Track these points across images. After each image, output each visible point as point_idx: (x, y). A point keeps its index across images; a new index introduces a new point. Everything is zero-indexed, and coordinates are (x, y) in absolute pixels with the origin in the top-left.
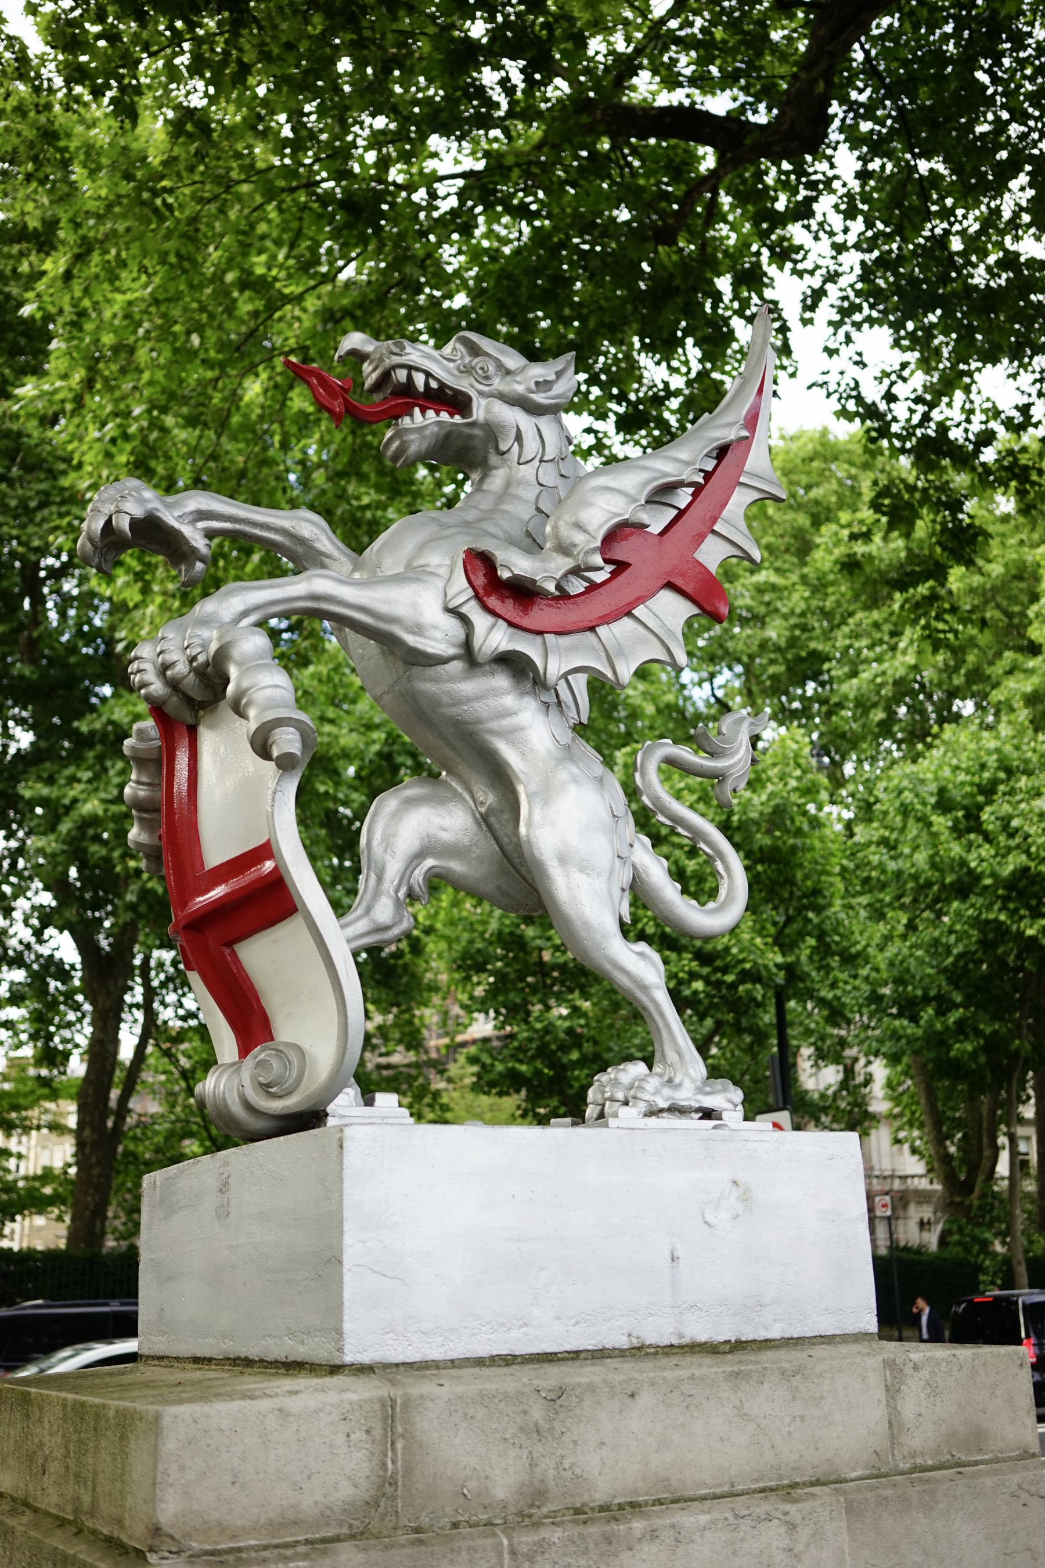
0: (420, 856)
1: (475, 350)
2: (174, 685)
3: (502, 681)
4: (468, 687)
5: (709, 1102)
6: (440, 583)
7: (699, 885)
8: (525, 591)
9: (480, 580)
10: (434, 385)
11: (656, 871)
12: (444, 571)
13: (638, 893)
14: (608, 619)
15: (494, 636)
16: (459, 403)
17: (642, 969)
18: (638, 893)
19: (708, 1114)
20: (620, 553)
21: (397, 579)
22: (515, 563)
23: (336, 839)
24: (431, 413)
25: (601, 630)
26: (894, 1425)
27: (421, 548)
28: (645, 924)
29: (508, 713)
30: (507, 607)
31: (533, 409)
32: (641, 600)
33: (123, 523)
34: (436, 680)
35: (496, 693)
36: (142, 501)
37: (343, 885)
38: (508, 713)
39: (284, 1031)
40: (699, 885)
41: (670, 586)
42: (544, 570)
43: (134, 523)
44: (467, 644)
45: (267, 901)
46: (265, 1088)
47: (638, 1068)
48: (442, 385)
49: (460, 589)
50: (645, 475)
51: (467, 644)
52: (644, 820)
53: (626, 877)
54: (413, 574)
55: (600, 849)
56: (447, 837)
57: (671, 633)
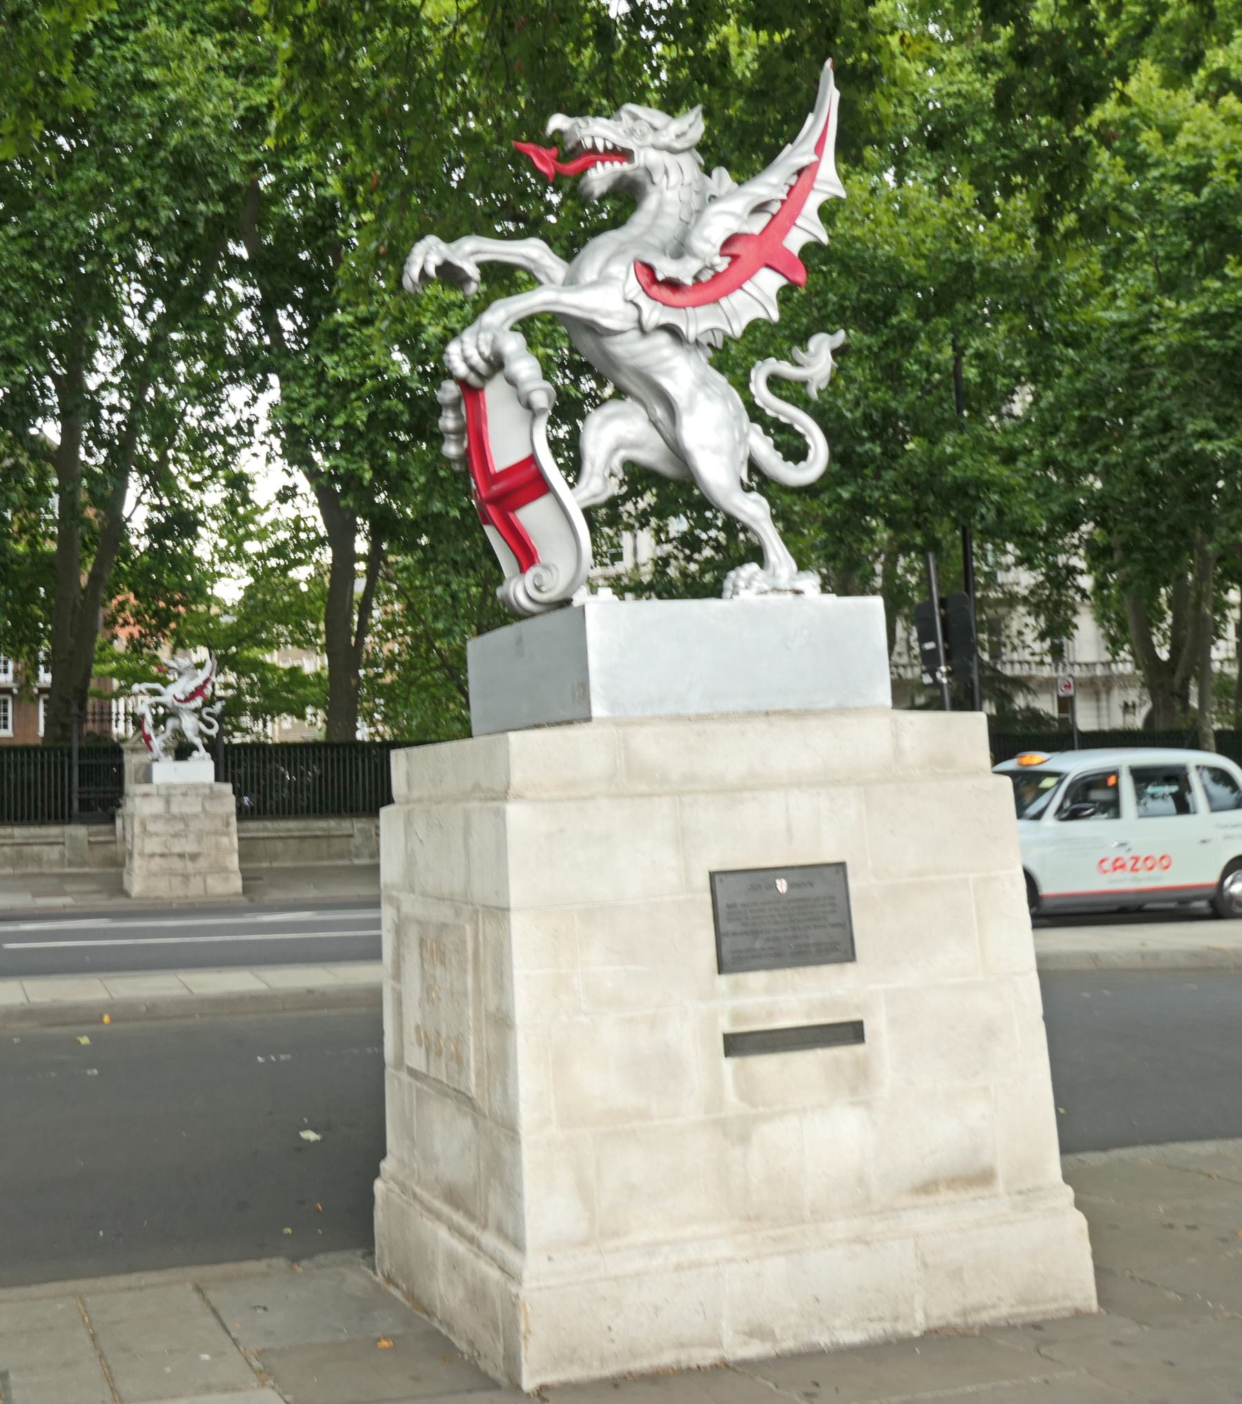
0: (616, 450)
1: (635, 118)
2: (472, 368)
3: (664, 338)
4: (642, 345)
5: (799, 585)
6: (620, 284)
7: (795, 451)
8: (673, 285)
9: (645, 279)
10: (610, 146)
11: (763, 447)
12: (622, 276)
13: (753, 467)
14: (726, 293)
15: (654, 314)
16: (624, 154)
17: (754, 510)
18: (753, 467)
19: (798, 592)
20: (735, 250)
21: (593, 284)
22: (666, 268)
23: (571, 456)
24: (608, 164)
25: (723, 301)
26: (898, 752)
27: (608, 262)
28: (758, 479)
29: (666, 359)
30: (665, 293)
31: (672, 151)
32: (749, 277)
33: (431, 271)
34: (621, 344)
35: (657, 348)
36: (439, 252)
37: (574, 467)
38: (666, 359)
39: (543, 555)
40: (795, 451)
41: (769, 266)
42: (684, 271)
43: (438, 269)
44: (639, 321)
45: (529, 482)
46: (538, 588)
47: (752, 568)
48: (615, 146)
49: (633, 287)
50: (748, 199)
51: (639, 321)
52: (755, 413)
53: (742, 455)
54: (603, 280)
55: (724, 438)
56: (631, 437)
57: (769, 298)
